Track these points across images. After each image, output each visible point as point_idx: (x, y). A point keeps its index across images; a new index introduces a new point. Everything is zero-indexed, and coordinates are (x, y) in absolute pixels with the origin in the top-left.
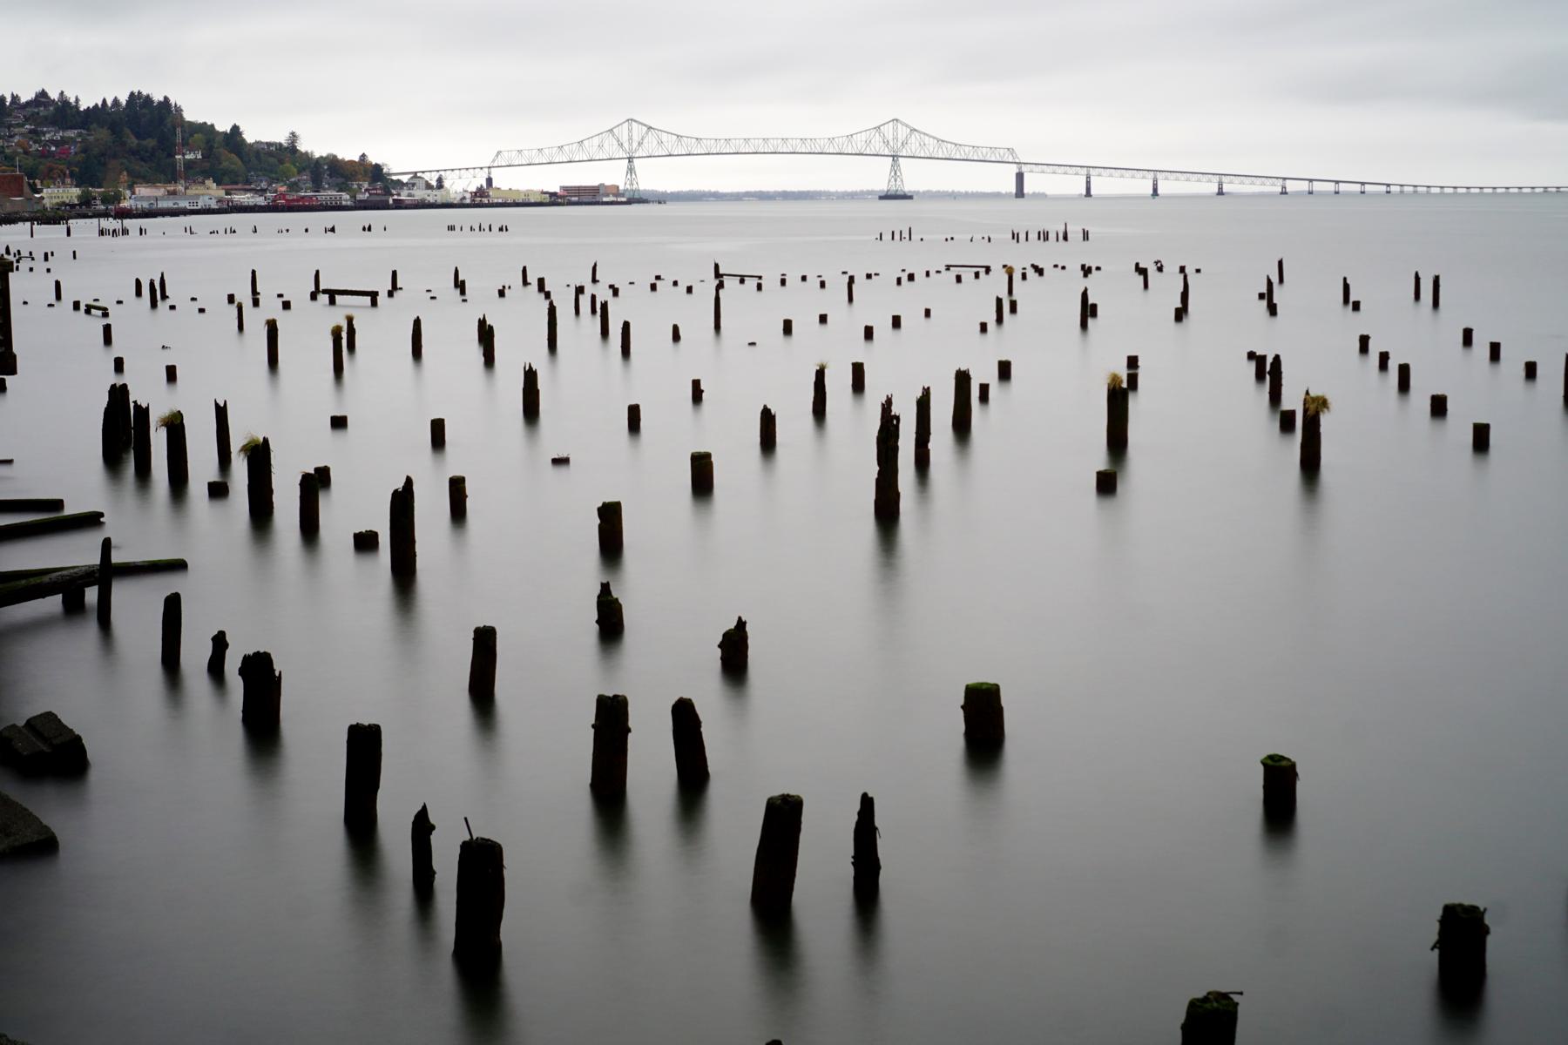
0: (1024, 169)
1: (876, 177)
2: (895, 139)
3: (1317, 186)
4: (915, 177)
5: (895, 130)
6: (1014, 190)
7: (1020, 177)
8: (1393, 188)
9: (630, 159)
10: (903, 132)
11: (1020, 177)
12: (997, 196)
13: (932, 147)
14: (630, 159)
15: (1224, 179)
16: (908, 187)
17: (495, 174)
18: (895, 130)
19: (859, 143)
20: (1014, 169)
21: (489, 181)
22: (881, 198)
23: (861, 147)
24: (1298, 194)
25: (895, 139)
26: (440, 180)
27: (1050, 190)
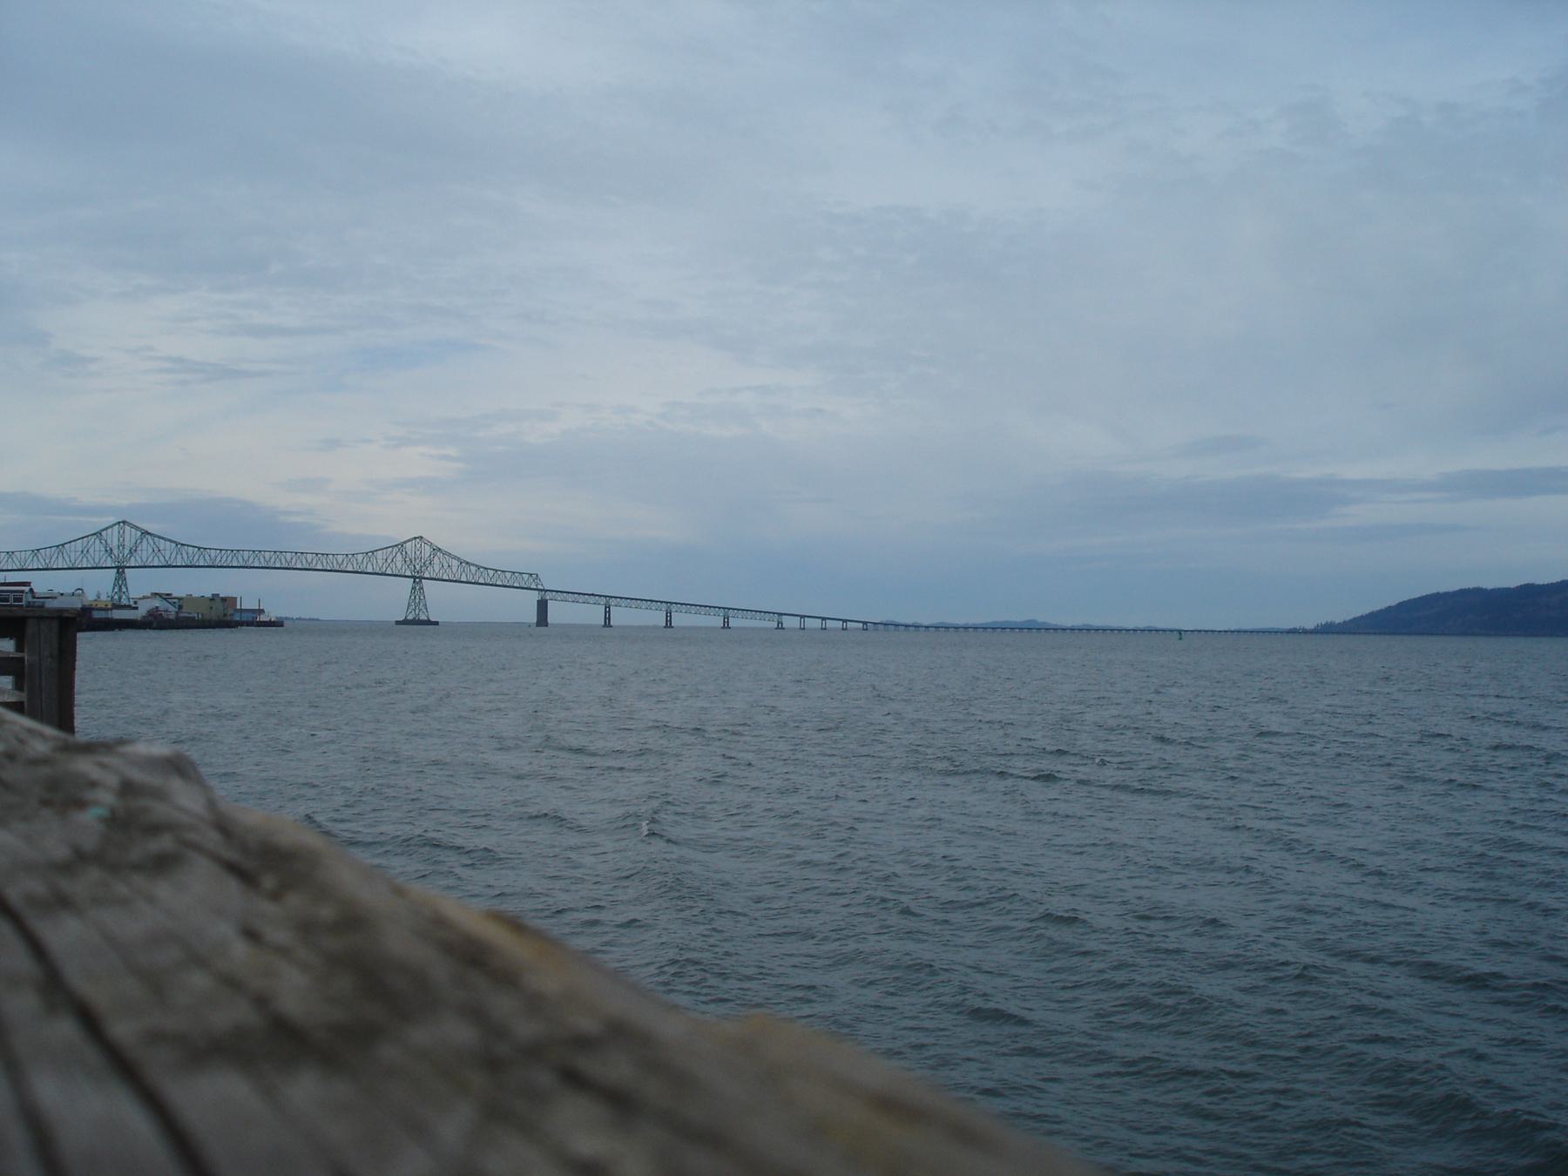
0: (548, 596)
1: (392, 599)
3: (809, 623)
4: (443, 601)
5: (122, 536)
7: (542, 606)
11: (542, 606)
14: (120, 569)
18: (122, 536)
19: (379, 562)
20: (535, 597)
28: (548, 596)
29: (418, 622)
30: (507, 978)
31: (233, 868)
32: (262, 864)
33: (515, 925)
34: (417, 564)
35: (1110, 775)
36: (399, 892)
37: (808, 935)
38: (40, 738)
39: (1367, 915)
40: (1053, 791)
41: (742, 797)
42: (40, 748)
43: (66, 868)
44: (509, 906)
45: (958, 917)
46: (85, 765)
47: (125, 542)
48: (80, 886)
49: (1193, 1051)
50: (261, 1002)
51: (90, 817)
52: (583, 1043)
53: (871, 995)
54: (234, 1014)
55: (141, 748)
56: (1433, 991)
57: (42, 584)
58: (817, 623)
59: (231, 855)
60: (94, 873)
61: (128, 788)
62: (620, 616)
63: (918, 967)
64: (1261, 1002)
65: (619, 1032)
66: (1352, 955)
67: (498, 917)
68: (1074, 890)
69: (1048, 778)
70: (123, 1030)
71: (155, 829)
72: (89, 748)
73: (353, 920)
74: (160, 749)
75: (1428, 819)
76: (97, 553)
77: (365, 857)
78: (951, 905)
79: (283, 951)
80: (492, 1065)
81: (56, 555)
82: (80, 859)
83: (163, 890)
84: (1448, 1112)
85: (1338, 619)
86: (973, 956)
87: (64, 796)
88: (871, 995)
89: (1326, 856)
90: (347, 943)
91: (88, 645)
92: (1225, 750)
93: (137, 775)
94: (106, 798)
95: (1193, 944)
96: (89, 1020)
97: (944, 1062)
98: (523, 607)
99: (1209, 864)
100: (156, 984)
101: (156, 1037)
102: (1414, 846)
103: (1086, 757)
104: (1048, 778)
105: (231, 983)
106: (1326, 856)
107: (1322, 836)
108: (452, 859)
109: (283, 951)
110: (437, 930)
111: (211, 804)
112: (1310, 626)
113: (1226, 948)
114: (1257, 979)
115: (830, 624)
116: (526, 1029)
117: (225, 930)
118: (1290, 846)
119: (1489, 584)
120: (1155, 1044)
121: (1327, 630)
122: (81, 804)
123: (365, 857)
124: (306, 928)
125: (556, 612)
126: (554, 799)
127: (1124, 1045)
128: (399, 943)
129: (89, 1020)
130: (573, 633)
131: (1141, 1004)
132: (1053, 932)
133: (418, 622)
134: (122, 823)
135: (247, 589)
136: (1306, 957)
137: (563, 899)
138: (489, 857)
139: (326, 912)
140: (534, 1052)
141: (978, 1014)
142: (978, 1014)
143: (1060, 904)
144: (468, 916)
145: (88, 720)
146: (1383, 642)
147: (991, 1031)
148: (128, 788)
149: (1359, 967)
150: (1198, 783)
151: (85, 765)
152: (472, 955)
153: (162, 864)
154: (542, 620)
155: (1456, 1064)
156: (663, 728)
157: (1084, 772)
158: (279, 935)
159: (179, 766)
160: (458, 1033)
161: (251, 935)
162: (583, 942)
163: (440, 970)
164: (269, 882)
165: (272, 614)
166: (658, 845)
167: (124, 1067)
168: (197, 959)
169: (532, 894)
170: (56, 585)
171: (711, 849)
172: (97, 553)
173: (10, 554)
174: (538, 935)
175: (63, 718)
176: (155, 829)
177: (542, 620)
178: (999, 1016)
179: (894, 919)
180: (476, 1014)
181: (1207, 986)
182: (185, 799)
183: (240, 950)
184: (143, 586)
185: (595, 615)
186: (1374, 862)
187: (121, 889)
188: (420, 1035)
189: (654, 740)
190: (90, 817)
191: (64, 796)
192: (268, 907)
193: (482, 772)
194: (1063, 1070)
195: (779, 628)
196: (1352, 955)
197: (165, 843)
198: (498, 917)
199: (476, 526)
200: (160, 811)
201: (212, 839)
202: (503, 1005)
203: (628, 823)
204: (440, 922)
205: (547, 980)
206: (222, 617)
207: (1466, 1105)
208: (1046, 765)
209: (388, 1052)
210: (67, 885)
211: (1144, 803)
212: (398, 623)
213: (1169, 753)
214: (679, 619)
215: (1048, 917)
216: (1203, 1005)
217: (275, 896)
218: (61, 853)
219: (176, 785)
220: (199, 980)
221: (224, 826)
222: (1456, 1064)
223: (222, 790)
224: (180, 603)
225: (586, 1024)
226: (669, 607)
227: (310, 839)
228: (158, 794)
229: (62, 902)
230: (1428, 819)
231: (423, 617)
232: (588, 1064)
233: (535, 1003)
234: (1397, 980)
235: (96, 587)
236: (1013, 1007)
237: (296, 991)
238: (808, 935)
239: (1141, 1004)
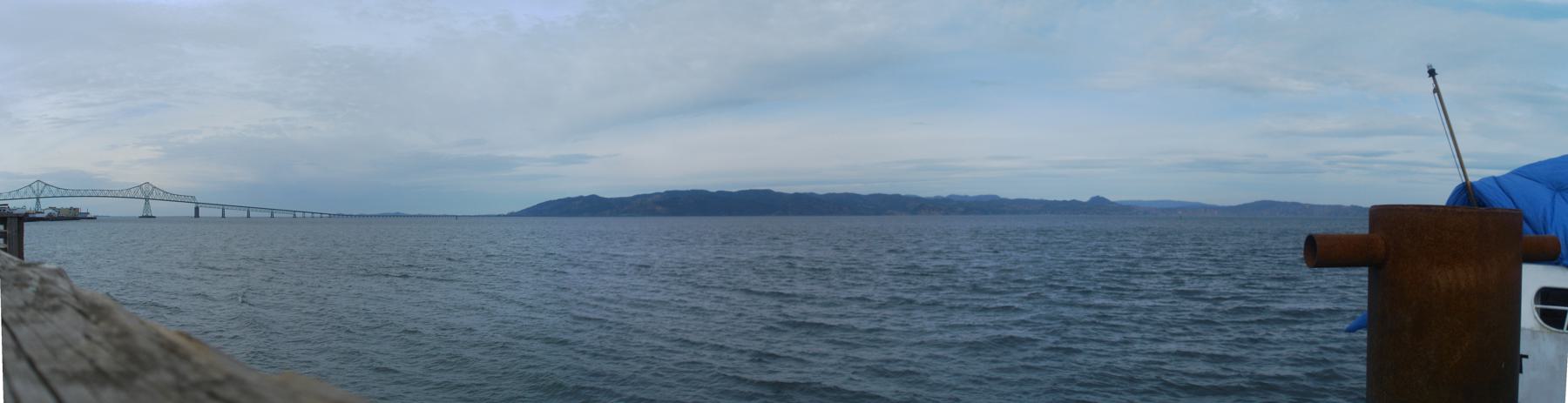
1: (137, 208)
4: (158, 208)
7: (197, 209)
11: (197, 209)
29: (147, 217)
30: (186, 357)
31: (80, 311)
32: (91, 311)
33: (189, 337)
34: (147, 194)
35: (429, 274)
36: (143, 323)
37: (308, 341)
38: (11, 260)
39: (526, 322)
40: (407, 281)
41: (279, 287)
42: (12, 265)
43: (22, 309)
44: (186, 330)
45: (369, 333)
46: (27, 272)
47: (39, 188)
48: (28, 315)
49: (462, 378)
50: (92, 361)
51: (30, 291)
52: (216, 383)
53: (335, 364)
54: (81, 365)
55: (47, 266)
56: (549, 347)
57: (12, 205)
59: (80, 307)
60: (32, 311)
61: (42, 281)
62: (228, 213)
63: (352, 353)
64: (487, 358)
65: (230, 379)
66: (521, 337)
67: (181, 334)
68: (415, 320)
69: (405, 276)
70: (43, 368)
71: (52, 296)
72: (29, 265)
73: (125, 333)
74: (53, 266)
75: (548, 285)
76: (30, 193)
77: (130, 309)
78: (367, 328)
79: (99, 344)
80: (180, 390)
81: (16, 194)
82: (27, 306)
83: (55, 318)
84: (556, 388)
85: (516, 209)
86: (376, 348)
87: (21, 283)
88: (335, 364)
89: (512, 301)
90: (123, 341)
91: (28, 227)
92: (474, 263)
93: (46, 276)
94: (35, 284)
95: (462, 338)
96: (32, 363)
97: (364, 388)
98: (189, 210)
99: (468, 307)
100: (54, 352)
101: (55, 371)
102: (543, 296)
103: (420, 267)
104: (405, 276)
105: (80, 354)
106: (512, 301)
107: (509, 294)
108: (163, 311)
109: (99, 344)
110: (158, 338)
111: (72, 287)
113: (475, 339)
114: (485, 349)
116: (193, 377)
117: (78, 335)
118: (498, 299)
120: (448, 376)
121: (511, 215)
122: (27, 286)
123: (130, 309)
124: (108, 335)
125: (203, 212)
126: (204, 289)
127: (436, 378)
128: (143, 343)
129: (32, 363)
130: (209, 220)
131: (443, 362)
132: (407, 337)
133: (147, 217)
134: (40, 293)
135: (83, 205)
136: (504, 340)
137: (208, 328)
138: (177, 310)
139: (115, 330)
140: (197, 385)
141: (378, 370)
142: (378, 370)
143: (410, 326)
144: (169, 333)
145: (29, 255)
146: (531, 219)
147: (382, 376)
148: (42, 281)
149: (523, 342)
150: (463, 276)
151: (27, 272)
152: (171, 348)
153: (55, 309)
154: (197, 215)
155: (557, 372)
156: (247, 259)
157: (419, 273)
158: (99, 338)
159: (60, 273)
160: (168, 378)
161: (87, 337)
162: (216, 344)
163: (159, 353)
164: (93, 317)
165: (92, 214)
166: (245, 306)
167: (44, 381)
168: (69, 345)
169: (194, 325)
170: (16, 205)
171: (268, 308)
172: (30, 193)
174: (197, 341)
175: (21, 255)
176: (52, 296)
177: (197, 215)
178: (387, 370)
179: (343, 335)
180: (173, 370)
181: (468, 354)
182: (63, 285)
183: (83, 342)
184: (46, 204)
185: (219, 213)
186: (529, 303)
187: (42, 317)
188: (152, 377)
189: (243, 264)
190: (30, 291)
191: (21, 283)
192: (94, 327)
193: (174, 277)
194: (412, 389)
195: (294, 217)
196: (521, 337)
197: (56, 301)
198: (181, 334)
199: (169, 178)
200: (54, 289)
201: (72, 300)
202: (184, 368)
203: (233, 297)
204: (158, 335)
205: (201, 358)
206: (74, 216)
207: (560, 386)
208: (404, 271)
209: (139, 383)
210: (22, 314)
211: (443, 284)
213: (453, 264)
214: (252, 214)
215: (406, 331)
216: (466, 360)
217: (96, 323)
218: (21, 303)
219: (59, 280)
220: (69, 352)
221: (76, 296)
222: (557, 372)
223: (76, 282)
224: (59, 211)
225: (218, 376)
226: (248, 209)
227: (108, 301)
228: (53, 283)
229: (21, 321)
230: (548, 285)
232: (218, 390)
233: (197, 367)
234: (537, 345)
235: (30, 205)
236: (392, 366)
237: (104, 359)
238: (308, 341)
239: (443, 362)
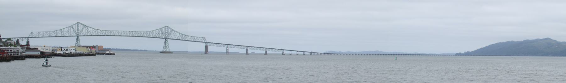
0: (208, 44)
1: (159, 45)
2: (78, 29)
3: (292, 52)
4: (173, 46)
5: (78, 27)
6: (204, 51)
7: (206, 47)
8: (285, 52)
9: (78, 37)
10: (81, 27)
11: (206, 47)
12: (155, 52)
13: (178, 37)
14: (78, 37)
15: (249, 48)
16: (171, 50)
17: (30, 40)
18: (78, 27)
20: (204, 44)
21: (28, 42)
22: (161, 52)
23: (155, 35)
24: (287, 54)
25: (78, 29)
26: (18, 41)
27: (190, 50)
28: (208, 44)
58: (303, 53)
76: (71, 32)
98: (201, 48)
112: (463, 52)
115: (292, 52)
119: (559, 40)
121: (468, 54)
125: (210, 49)
173: (54, 32)
184: (86, 42)
212: (161, 52)
231: (168, 50)
